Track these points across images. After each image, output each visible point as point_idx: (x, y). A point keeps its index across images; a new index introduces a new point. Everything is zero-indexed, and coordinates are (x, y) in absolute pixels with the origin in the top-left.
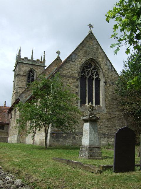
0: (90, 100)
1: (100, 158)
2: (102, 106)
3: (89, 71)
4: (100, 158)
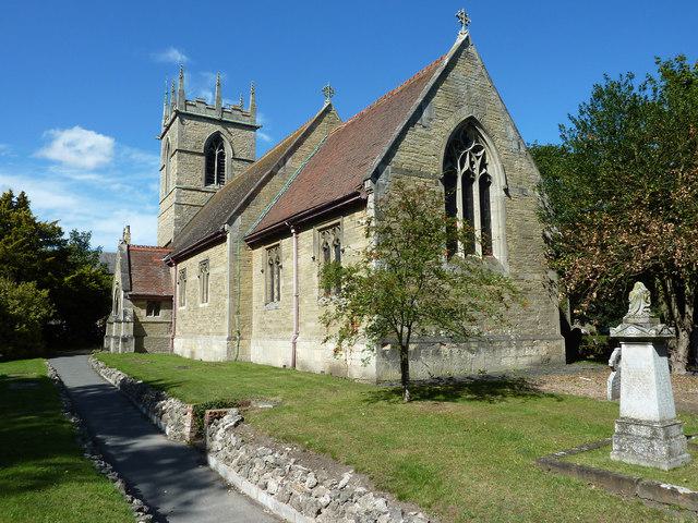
0: (470, 249)
1: (478, 234)
2: (497, 258)
3: (466, 154)
4: (478, 234)
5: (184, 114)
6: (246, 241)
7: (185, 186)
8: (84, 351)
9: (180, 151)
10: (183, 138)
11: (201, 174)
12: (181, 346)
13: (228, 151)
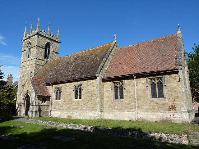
5: (39, 34)
6: (102, 79)
7: (38, 58)
8: (80, 127)
9: (37, 46)
10: (38, 42)
11: (43, 55)
12: (55, 114)
13: (51, 48)
